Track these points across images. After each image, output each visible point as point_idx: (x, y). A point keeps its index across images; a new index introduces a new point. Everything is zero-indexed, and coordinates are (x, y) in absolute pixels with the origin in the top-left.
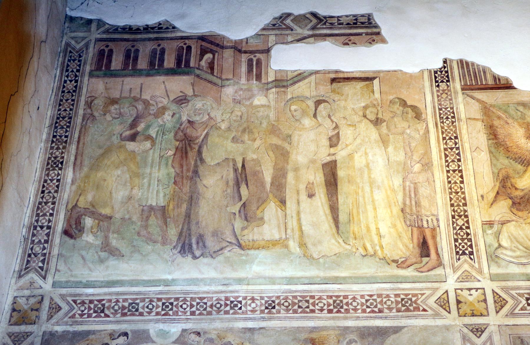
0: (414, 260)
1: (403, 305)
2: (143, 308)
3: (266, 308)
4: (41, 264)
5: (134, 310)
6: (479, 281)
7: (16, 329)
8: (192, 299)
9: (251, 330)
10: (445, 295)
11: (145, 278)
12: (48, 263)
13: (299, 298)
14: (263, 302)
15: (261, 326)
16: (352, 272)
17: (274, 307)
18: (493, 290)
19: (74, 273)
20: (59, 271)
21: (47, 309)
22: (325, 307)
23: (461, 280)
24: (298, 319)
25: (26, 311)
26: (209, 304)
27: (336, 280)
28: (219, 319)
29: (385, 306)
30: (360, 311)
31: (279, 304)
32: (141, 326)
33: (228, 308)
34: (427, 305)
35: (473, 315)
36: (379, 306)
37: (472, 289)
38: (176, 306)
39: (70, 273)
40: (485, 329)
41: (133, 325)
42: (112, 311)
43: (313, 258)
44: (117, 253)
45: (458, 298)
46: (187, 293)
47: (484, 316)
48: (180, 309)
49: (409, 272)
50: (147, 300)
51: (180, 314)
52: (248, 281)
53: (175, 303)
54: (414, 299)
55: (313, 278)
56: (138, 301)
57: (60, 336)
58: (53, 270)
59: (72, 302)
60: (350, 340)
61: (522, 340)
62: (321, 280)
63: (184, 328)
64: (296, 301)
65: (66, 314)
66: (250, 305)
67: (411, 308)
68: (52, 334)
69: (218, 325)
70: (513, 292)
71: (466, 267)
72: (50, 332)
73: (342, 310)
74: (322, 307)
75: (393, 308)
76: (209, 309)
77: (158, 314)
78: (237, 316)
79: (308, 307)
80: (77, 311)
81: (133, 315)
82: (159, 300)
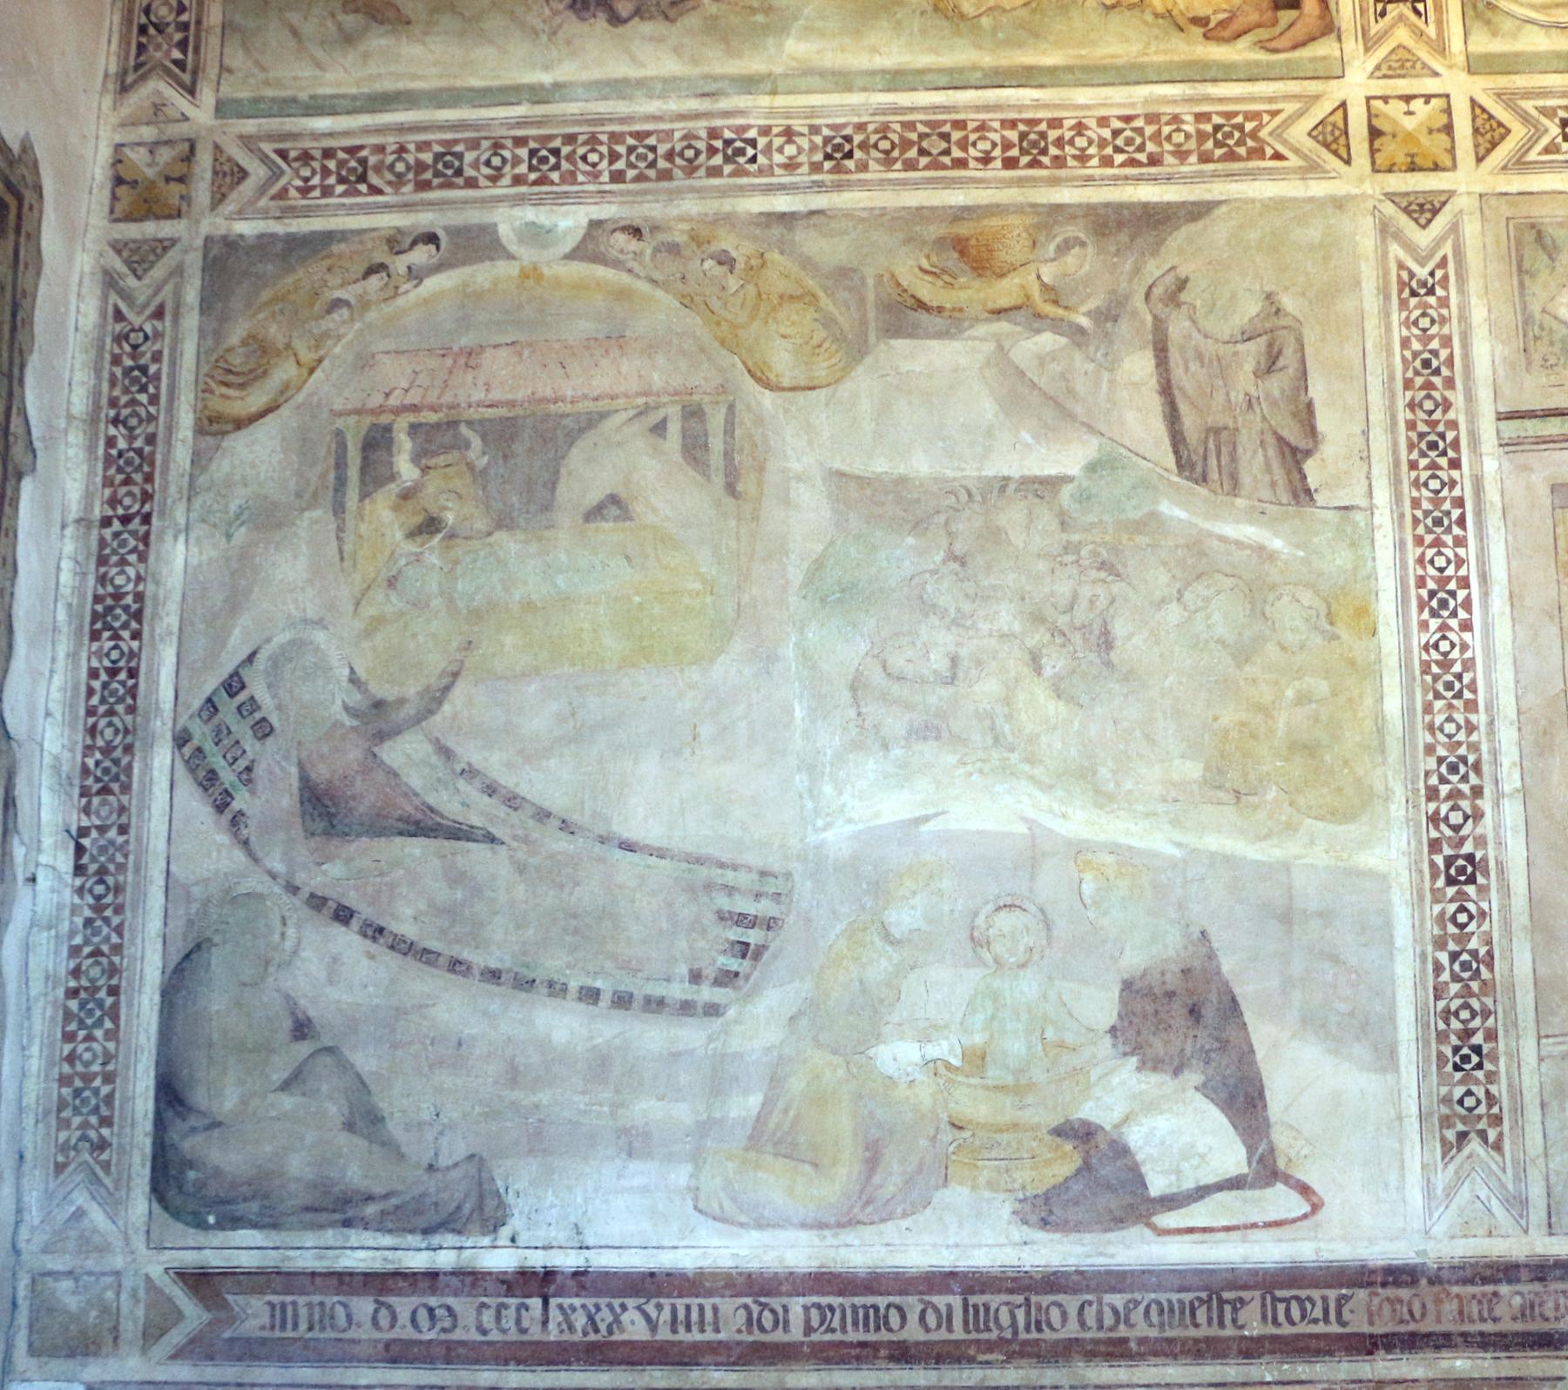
0: (1254, 17)
1: (1218, 144)
2: (475, 165)
3: (828, 157)
4: (176, 54)
5: (449, 172)
6: (1436, 74)
7: (133, 231)
8: (615, 137)
9: (786, 219)
10: (1340, 113)
11: (475, 82)
12: (197, 50)
13: (921, 128)
14: (818, 140)
15: (814, 207)
16: (1071, 52)
17: (849, 155)
18: (1473, 101)
19: (271, 75)
20: (230, 71)
21: (208, 175)
22: (997, 152)
23: (1384, 71)
24: (916, 184)
25: (153, 182)
26: (663, 149)
27: (1027, 76)
28: (693, 190)
29: (1168, 147)
30: (1095, 162)
31: (863, 146)
32: (474, 216)
33: (718, 160)
34: (1285, 142)
35: (1413, 168)
36: (1151, 147)
37: (1414, 97)
38: (569, 158)
39: (262, 76)
40: (1444, 204)
41: (450, 214)
42: (389, 176)
43: (962, 16)
44: (391, 14)
45: (1375, 122)
46: (601, 121)
47: (1444, 170)
48: (582, 166)
49: (1240, 52)
50: (485, 144)
51: (581, 178)
52: (774, 82)
53: (565, 150)
54: (1249, 126)
55: (961, 70)
56: (459, 148)
57: (253, 247)
58: (212, 71)
59: (274, 156)
60: (1066, 241)
61: (1539, 233)
62: (985, 76)
63: (595, 217)
64: (914, 136)
65: (262, 190)
66: (780, 150)
67: (1242, 151)
68: (231, 244)
69: (691, 206)
70: (1528, 105)
71: (1402, 35)
72: (224, 238)
73: (1045, 160)
74: (987, 153)
75: (1189, 152)
76: (662, 164)
77: (518, 180)
78: (744, 181)
79: (947, 152)
80: (290, 178)
81: (448, 185)
82: (520, 142)
